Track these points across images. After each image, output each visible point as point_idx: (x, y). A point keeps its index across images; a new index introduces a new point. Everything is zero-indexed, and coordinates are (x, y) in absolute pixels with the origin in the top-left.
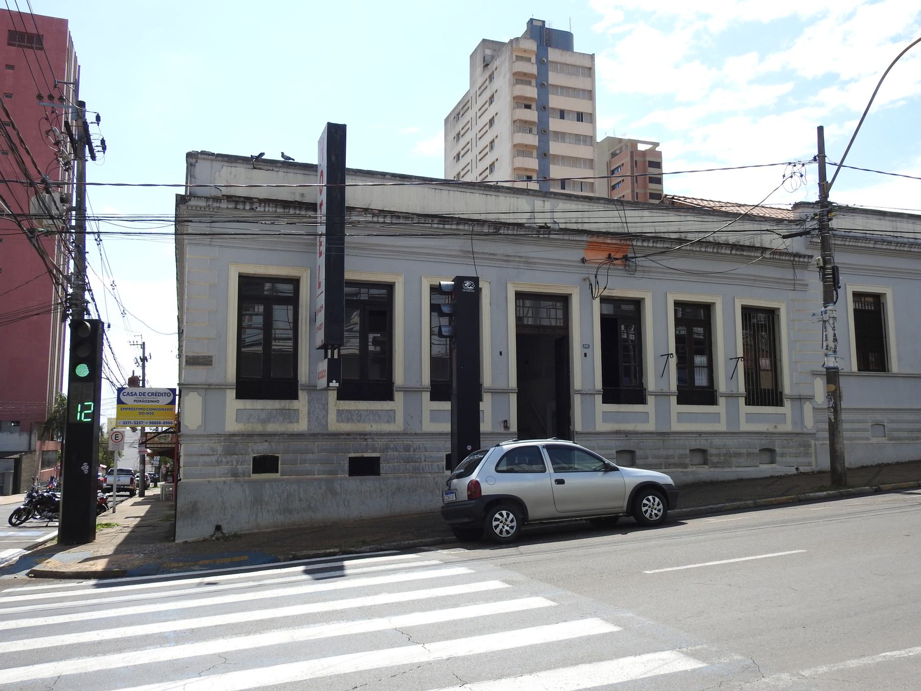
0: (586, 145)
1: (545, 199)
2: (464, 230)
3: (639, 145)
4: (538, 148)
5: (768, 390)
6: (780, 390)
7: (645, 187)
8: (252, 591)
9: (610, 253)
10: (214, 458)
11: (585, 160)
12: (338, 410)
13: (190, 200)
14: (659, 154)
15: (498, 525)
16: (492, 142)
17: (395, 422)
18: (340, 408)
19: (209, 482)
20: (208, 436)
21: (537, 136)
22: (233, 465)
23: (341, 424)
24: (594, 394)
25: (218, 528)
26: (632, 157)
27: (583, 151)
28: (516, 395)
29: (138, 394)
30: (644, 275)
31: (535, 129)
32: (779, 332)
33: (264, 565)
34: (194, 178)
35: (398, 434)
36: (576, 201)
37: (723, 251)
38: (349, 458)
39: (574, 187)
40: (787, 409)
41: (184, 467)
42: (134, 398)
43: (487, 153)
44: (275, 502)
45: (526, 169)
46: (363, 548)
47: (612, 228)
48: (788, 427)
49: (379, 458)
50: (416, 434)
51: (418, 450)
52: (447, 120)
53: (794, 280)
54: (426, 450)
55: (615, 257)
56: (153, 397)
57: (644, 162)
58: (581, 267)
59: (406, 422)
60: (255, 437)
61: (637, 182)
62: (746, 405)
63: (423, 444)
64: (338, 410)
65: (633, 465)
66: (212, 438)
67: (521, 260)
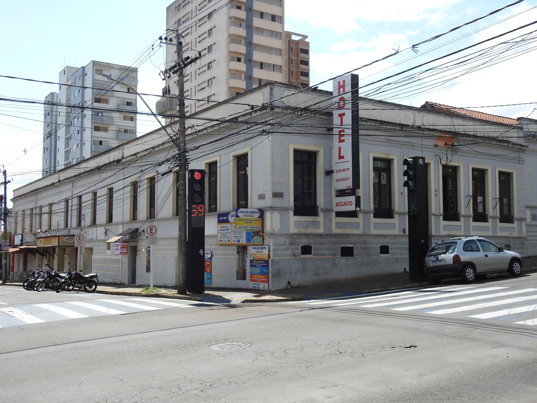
0: (277, 39)
1: (419, 112)
2: (383, 128)
3: (292, 36)
4: (245, 38)
5: (507, 215)
6: (512, 215)
7: (298, 67)
8: (379, 303)
9: (446, 142)
10: (285, 247)
11: (277, 49)
12: (336, 222)
13: (275, 109)
14: (308, 44)
15: (468, 275)
16: (210, 30)
17: (359, 229)
18: (337, 221)
19: (284, 259)
20: (283, 235)
21: (245, 30)
22: (293, 250)
23: (337, 229)
24: (440, 216)
25: (289, 283)
26: (289, 44)
27: (277, 43)
28: (408, 215)
29: (245, 212)
30: (462, 154)
31: (244, 24)
32: (512, 185)
33: (337, 298)
34: (273, 96)
35: (361, 235)
36: (432, 114)
37: (493, 143)
38: (341, 247)
39: (269, 68)
40: (515, 225)
41: (273, 251)
42: (243, 214)
43: (206, 38)
44: (312, 270)
45: (238, 53)
46: (393, 288)
47: (447, 129)
48: (515, 234)
49: (353, 247)
50: (369, 235)
51: (369, 243)
52: (168, 9)
53: (519, 158)
54: (372, 244)
55: (448, 144)
56: (251, 214)
57: (298, 49)
58: (434, 149)
59: (364, 229)
60: (303, 236)
61: (292, 63)
62: (500, 222)
63: (371, 240)
64: (336, 222)
65: (509, 250)
66: (285, 236)
67: (410, 144)
